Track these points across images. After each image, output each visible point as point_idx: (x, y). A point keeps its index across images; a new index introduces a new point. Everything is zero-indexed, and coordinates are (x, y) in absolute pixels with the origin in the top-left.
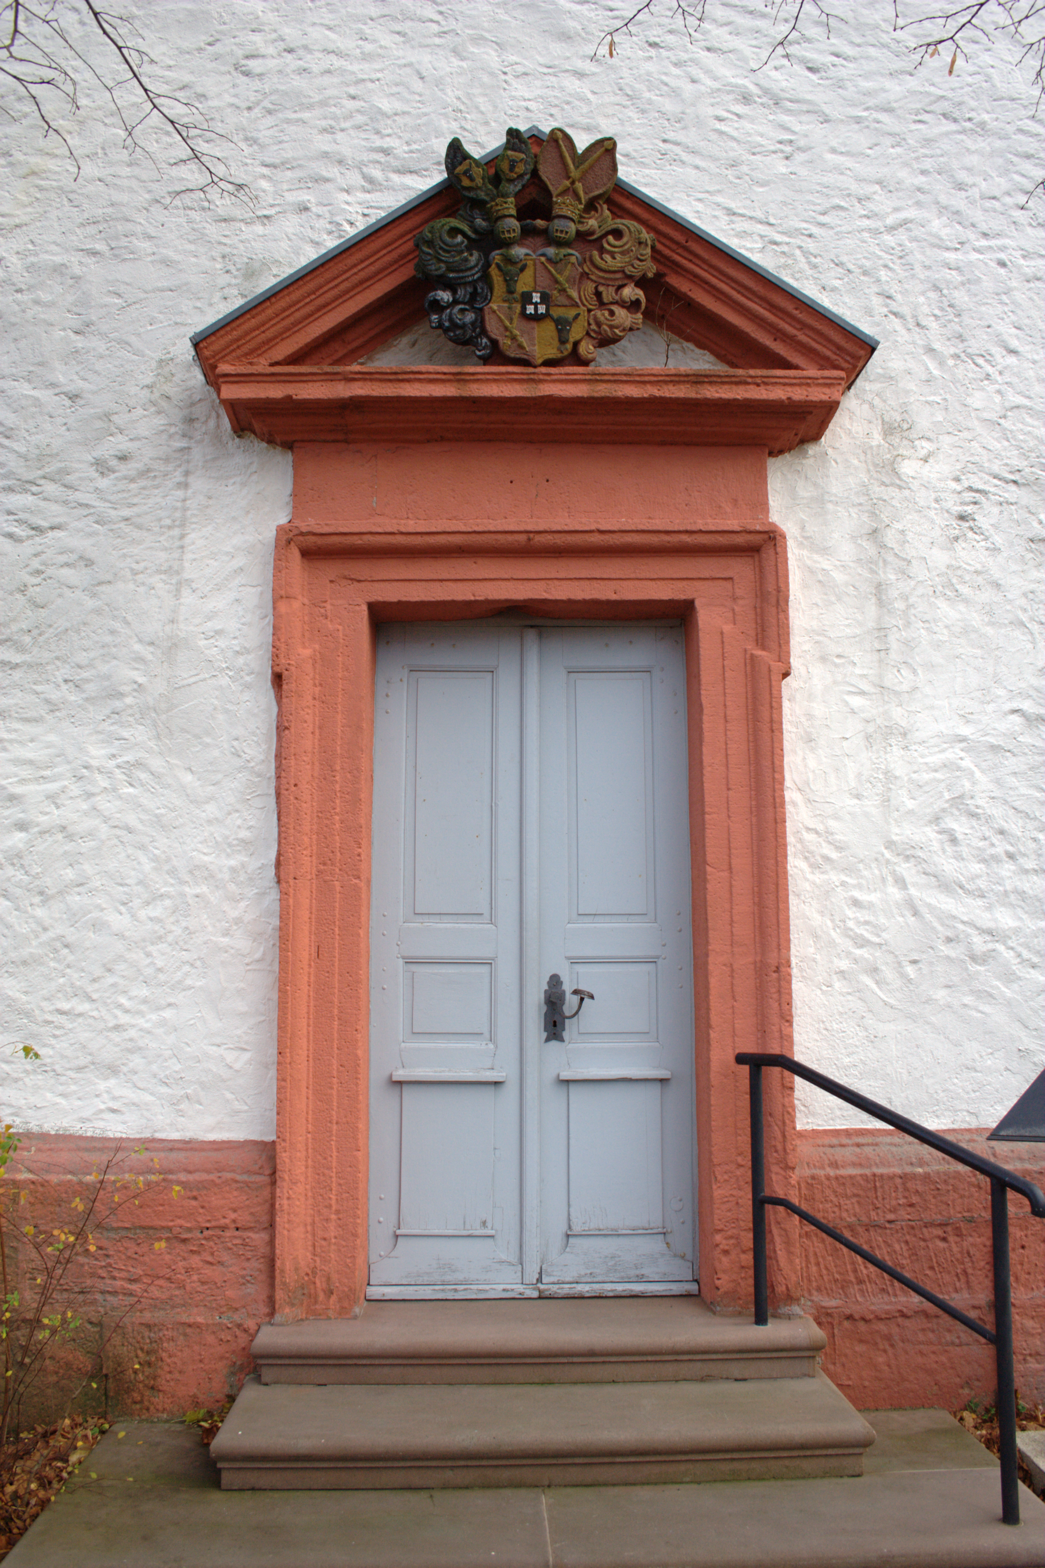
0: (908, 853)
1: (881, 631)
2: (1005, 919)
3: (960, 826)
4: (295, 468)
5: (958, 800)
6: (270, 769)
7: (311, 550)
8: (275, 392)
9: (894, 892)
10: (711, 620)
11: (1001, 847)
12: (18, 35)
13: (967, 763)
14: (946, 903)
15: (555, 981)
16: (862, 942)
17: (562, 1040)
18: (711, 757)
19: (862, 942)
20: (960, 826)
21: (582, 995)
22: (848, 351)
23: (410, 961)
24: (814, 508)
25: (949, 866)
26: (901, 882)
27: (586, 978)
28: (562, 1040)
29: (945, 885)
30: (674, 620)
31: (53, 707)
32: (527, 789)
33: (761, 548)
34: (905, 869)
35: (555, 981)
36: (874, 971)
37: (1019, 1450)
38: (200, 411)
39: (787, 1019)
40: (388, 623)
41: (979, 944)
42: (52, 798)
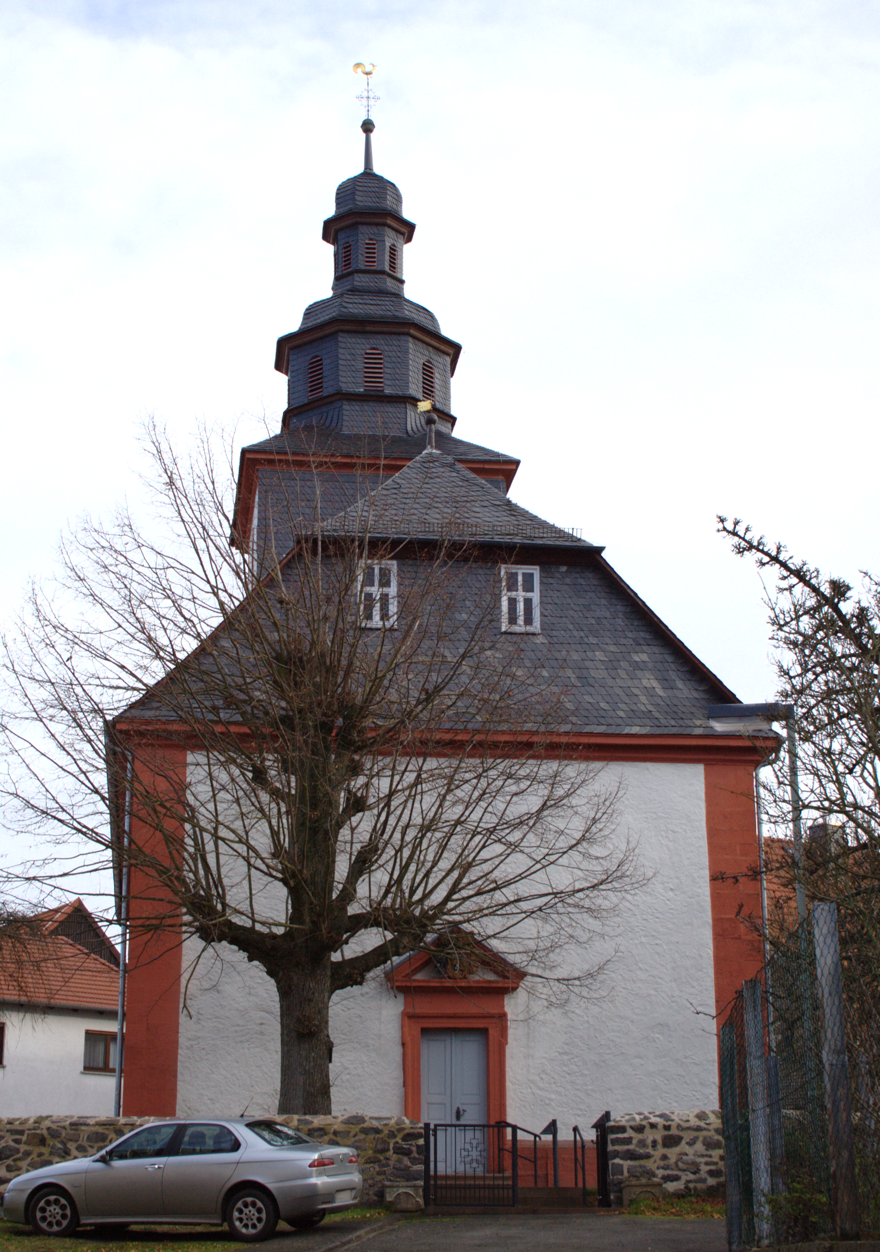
0: (533, 1082)
1: (528, 1034)
2: (553, 1096)
3: (544, 1076)
4: (405, 998)
5: (543, 1071)
6: (401, 1063)
7: (408, 1017)
8: (404, 984)
9: (529, 1090)
10: (491, 1032)
11: (552, 1081)
12: (117, 625)
13: (546, 1063)
14: (540, 1093)
15: (458, 1108)
16: (522, 1101)
17: (593, 1127)
18: (491, 1062)
19: (522, 1101)
20: (544, 1076)
21: (464, 1111)
22: (517, 463)
23: (428, 1103)
24: (514, 1006)
25: (541, 1085)
26: (531, 1088)
27: (465, 1107)
28: (593, 1127)
29: (540, 1089)
30: (484, 1032)
31: (354, 1049)
32: (452, 1068)
33: (503, 1016)
34: (532, 1085)
35: (458, 1108)
36: (525, 1106)
37: (302, 324)
38: (384, 983)
39: (505, 1115)
40: (425, 1031)
41: (547, 1101)
42: (355, 1068)
